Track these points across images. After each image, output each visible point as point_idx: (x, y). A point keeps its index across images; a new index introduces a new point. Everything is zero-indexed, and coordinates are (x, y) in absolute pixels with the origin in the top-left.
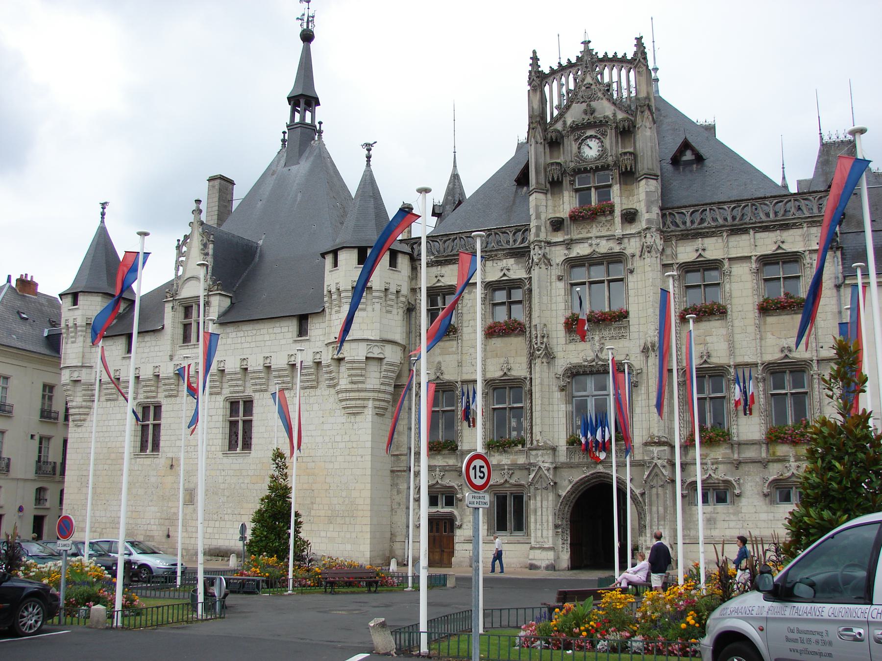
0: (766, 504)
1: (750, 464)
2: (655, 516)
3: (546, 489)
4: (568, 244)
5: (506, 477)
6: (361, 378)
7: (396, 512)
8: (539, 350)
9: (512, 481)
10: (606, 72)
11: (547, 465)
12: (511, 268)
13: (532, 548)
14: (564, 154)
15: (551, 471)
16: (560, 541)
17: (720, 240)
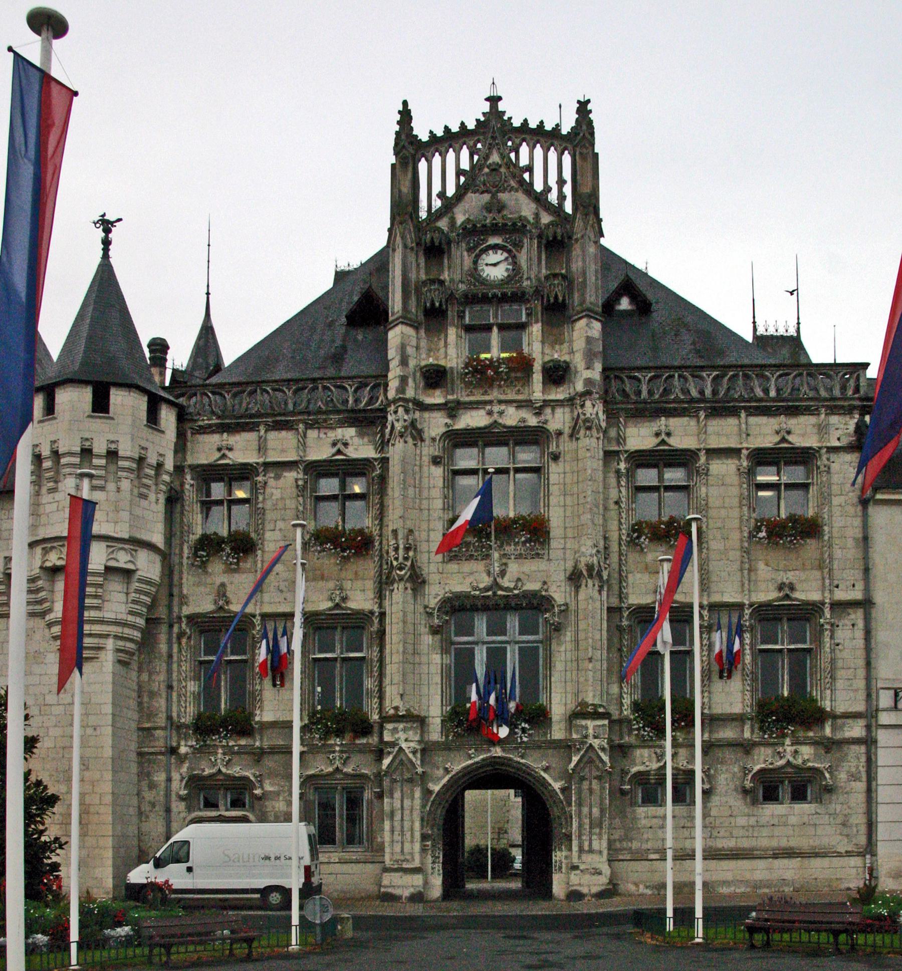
0: (746, 804)
1: (725, 749)
2: (587, 821)
3: (411, 781)
4: (453, 409)
5: (338, 763)
6: (95, 601)
7: (147, 817)
8: (401, 569)
9: (348, 770)
10: (524, 149)
11: (412, 745)
12: (350, 442)
13: (386, 870)
14: (449, 268)
15: (419, 755)
16: (429, 859)
17: (693, 422)
